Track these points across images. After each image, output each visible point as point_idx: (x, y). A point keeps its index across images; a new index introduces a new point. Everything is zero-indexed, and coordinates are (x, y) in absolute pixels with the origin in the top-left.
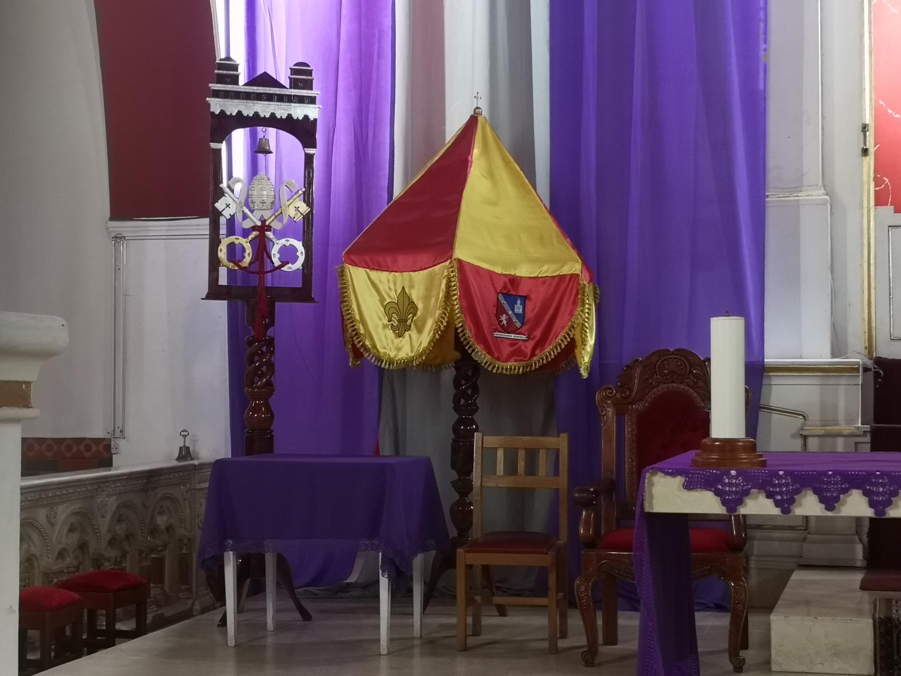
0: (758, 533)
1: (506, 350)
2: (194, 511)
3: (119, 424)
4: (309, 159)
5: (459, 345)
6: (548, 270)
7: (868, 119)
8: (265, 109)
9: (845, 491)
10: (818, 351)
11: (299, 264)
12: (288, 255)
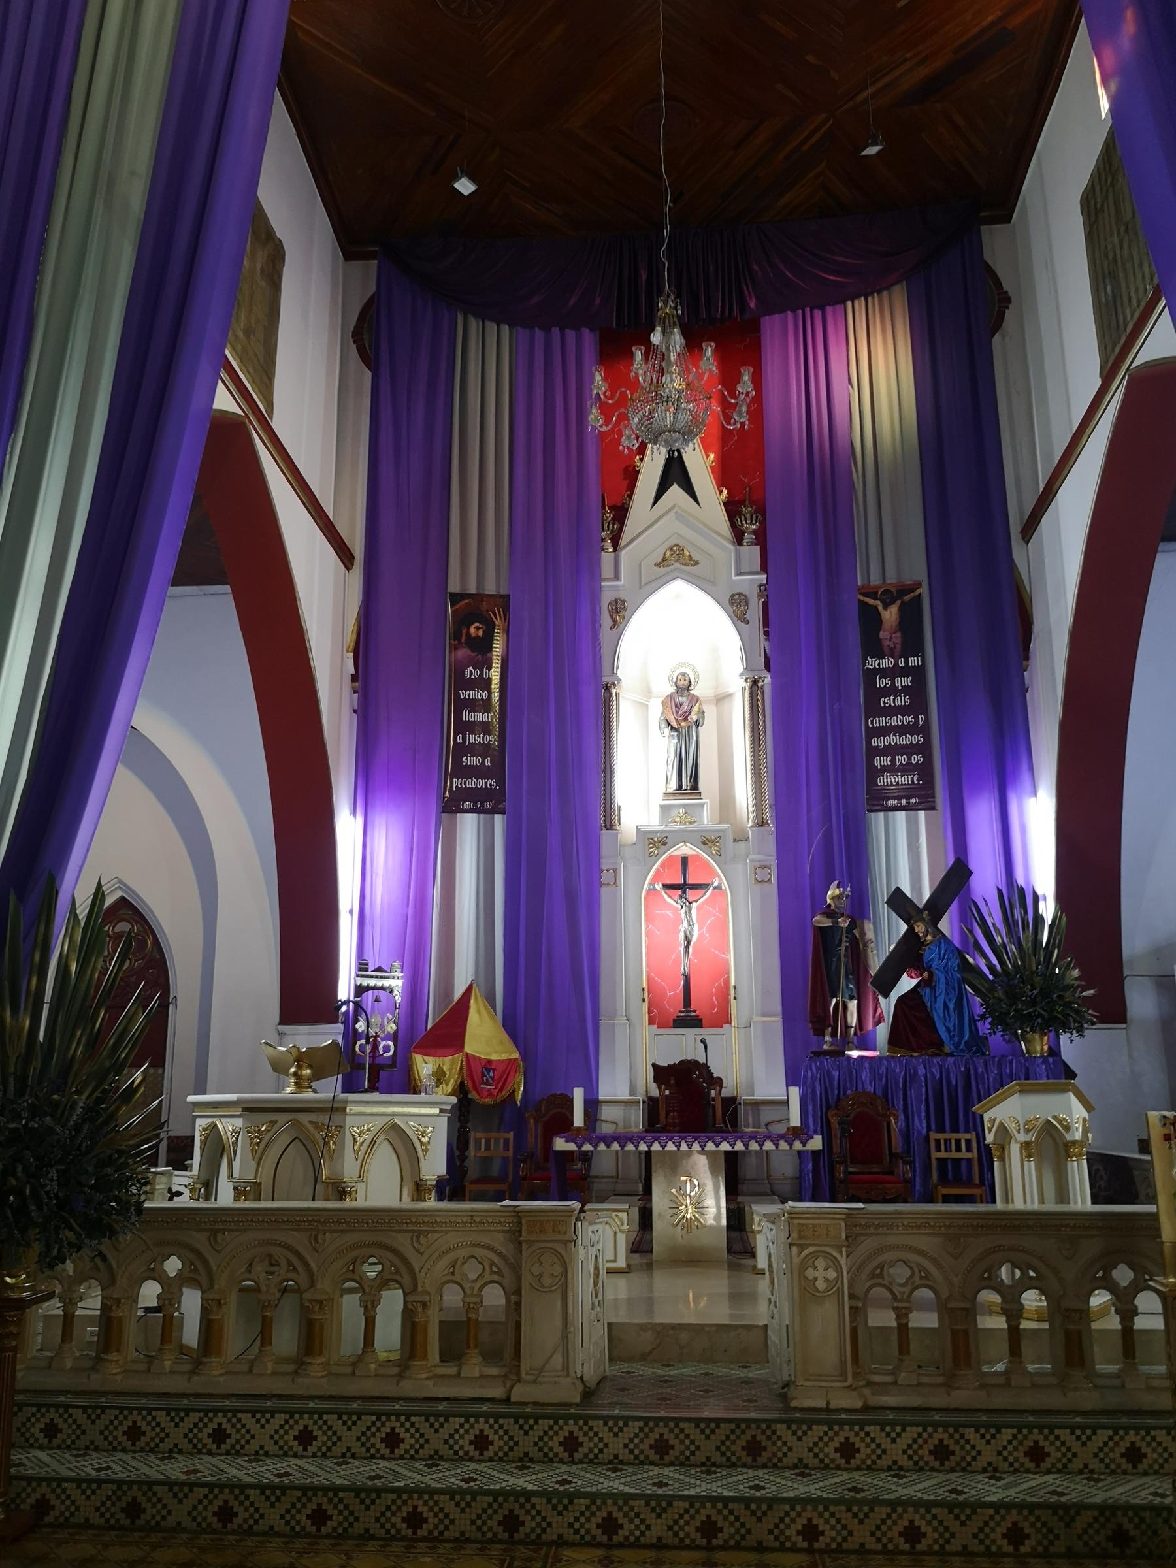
1: (486, 1094)
6: (504, 1057)
10: (624, 1095)
11: (391, 1053)
12: (387, 1049)
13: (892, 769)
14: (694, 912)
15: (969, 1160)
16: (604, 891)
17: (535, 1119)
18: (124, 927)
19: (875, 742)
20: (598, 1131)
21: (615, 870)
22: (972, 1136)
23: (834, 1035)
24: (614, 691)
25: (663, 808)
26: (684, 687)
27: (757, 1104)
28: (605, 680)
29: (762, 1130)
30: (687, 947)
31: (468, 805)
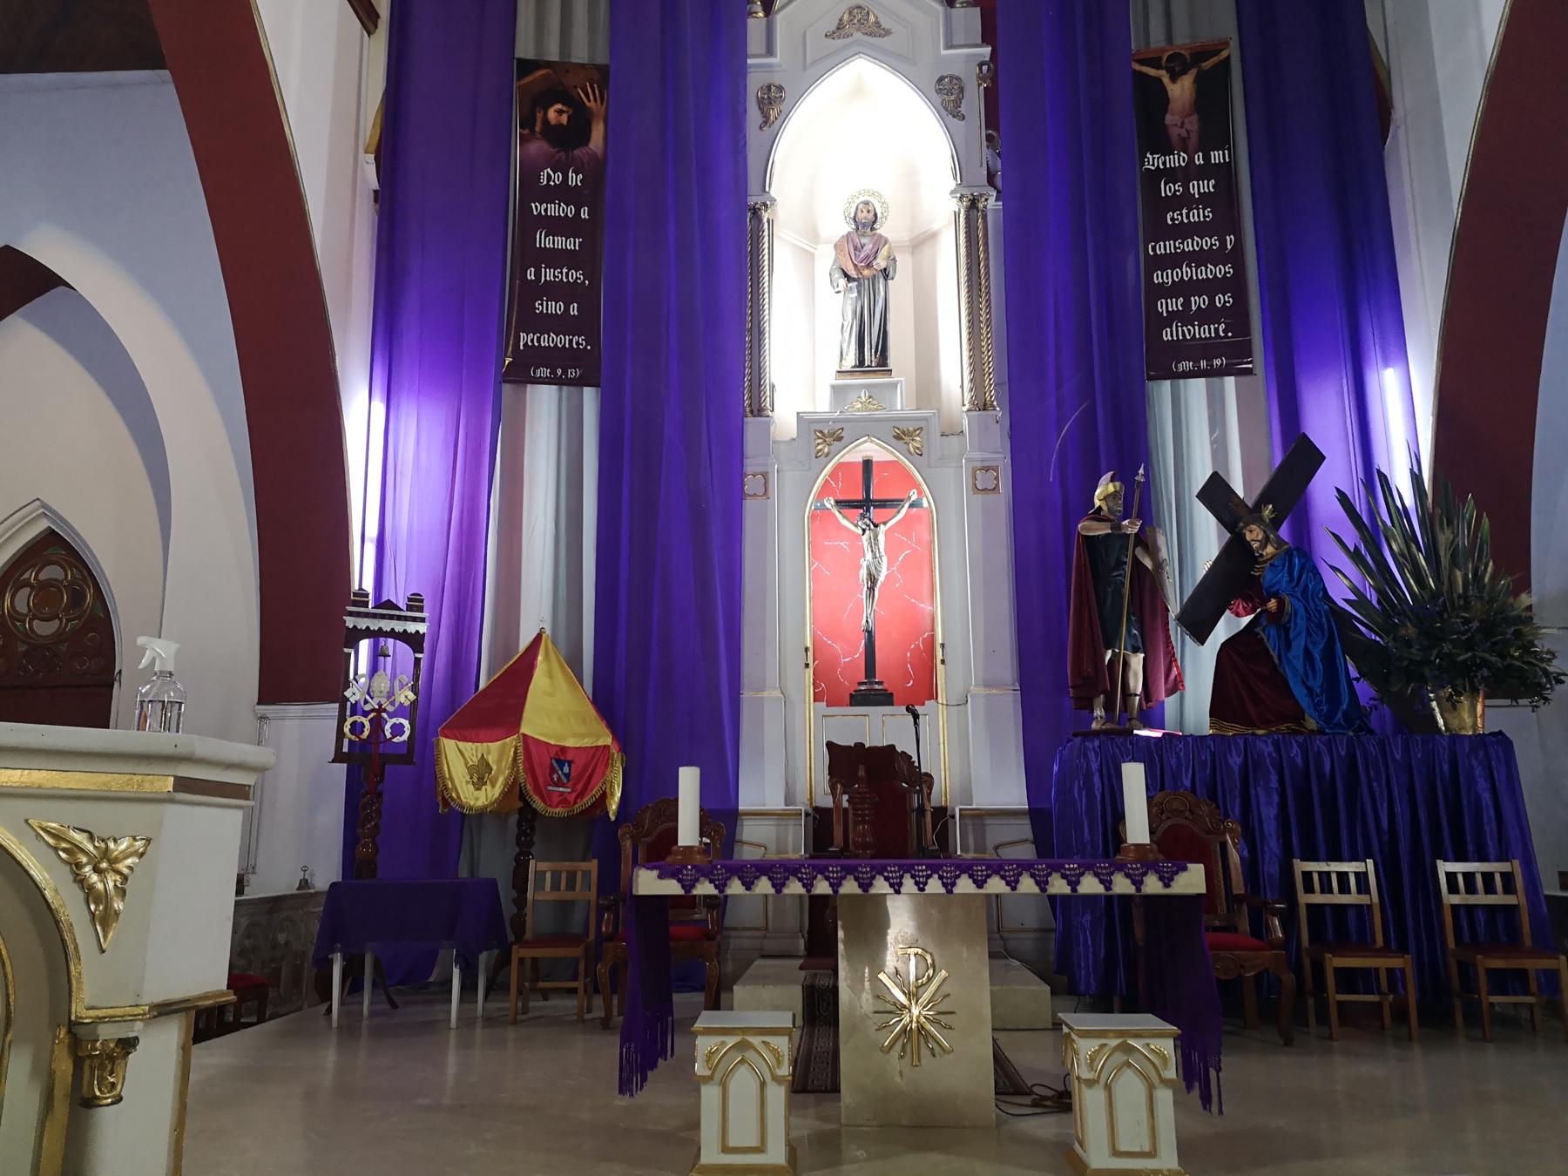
0: (733, 933)
1: (556, 799)
2: (311, 927)
3: (252, 862)
4: (417, 661)
5: (522, 796)
6: (587, 742)
7: (809, 644)
8: (387, 625)
9: (757, 878)
10: (776, 802)
11: (405, 737)
12: (398, 730)
13: (1184, 317)
14: (882, 538)
15: (1510, 910)
16: (750, 506)
17: (632, 838)
18: (52, 572)
19: (1158, 278)
20: (736, 857)
21: (765, 475)
22: (1514, 867)
23: (1109, 707)
24: (765, 216)
25: (835, 389)
26: (866, 222)
27: (979, 817)
28: (751, 201)
29: (990, 855)
30: (871, 589)
31: (543, 372)
